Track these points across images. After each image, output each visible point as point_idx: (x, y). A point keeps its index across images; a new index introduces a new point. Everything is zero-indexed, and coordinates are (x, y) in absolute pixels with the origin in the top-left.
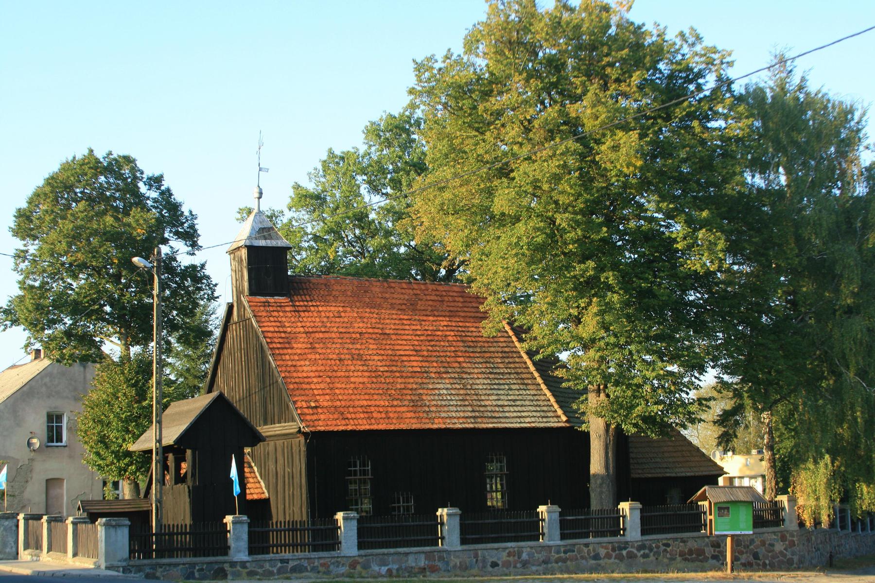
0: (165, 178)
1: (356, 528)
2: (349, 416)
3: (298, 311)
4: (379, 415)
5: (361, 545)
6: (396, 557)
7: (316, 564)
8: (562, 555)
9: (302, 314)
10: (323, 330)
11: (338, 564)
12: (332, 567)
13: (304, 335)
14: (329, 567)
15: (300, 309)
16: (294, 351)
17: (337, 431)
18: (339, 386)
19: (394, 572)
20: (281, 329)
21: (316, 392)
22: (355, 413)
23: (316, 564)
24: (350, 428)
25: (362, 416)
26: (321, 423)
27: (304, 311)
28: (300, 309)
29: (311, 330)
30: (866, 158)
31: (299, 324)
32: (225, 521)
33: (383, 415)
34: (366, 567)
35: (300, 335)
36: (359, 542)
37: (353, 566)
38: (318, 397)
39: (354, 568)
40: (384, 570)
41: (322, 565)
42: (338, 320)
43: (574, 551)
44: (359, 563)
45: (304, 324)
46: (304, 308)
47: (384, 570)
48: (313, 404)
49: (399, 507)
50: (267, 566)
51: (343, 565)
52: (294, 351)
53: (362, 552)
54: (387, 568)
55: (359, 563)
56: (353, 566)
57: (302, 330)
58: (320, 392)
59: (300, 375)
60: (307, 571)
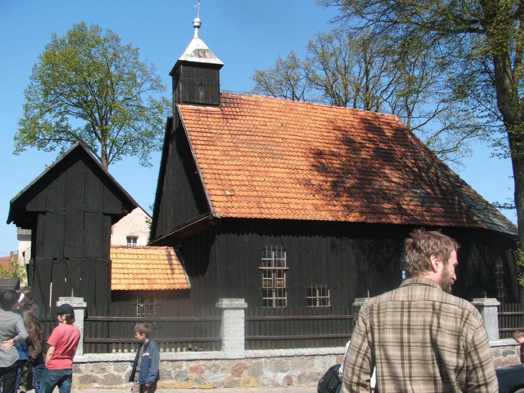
0: (12, 145)
1: (243, 320)
2: (264, 205)
3: (227, 119)
4: (296, 207)
5: (251, 342)
6: (296, 360)
7: (184, 368)
8: (501, 357)
9: (230, 121)
10: (248, 133)
11: (216, 369)
12: (207, 372)
13: (230, 136)
14: (202, 372)
15: (229, 117)
16: (217, 148)
17: (251, 219)
18: (258, 179)
19: (295, 379)
20: (207, 130)
21: (233, 183)
22: (271, 203)
23: (184, 368)
24: (264, 216)
25: (278, 206)
26: (234, 210)
27: (232, 119)
28: (229, 117)
29: (236, 132)
30: (521, 97)
31: (226, 128)
32: (60, 298)
33: (300, 207)
34: (256, 373)
35: (225, 136)
36: (246, 340)
37: (237, 371)
38: (234, 187)
39: (239, 375)
40: (281, 377)
41: (193, 370)
42: (263, 127)
43: (513, 353)
44: (245, 368)
45: (230, 128)
46: (233, 117)
47: (281, 377)
48: (228, 193)
49: (315, 300)
50: (111, 369)
51: (223, 369)
52: (217, 148)
53: (252, 353)
54: (284, 375)
55: (245, 368)
56: (237, 371)
57: (228, 132)
58: (238, 183)
59: (219, 167)
60: (171, 378)
